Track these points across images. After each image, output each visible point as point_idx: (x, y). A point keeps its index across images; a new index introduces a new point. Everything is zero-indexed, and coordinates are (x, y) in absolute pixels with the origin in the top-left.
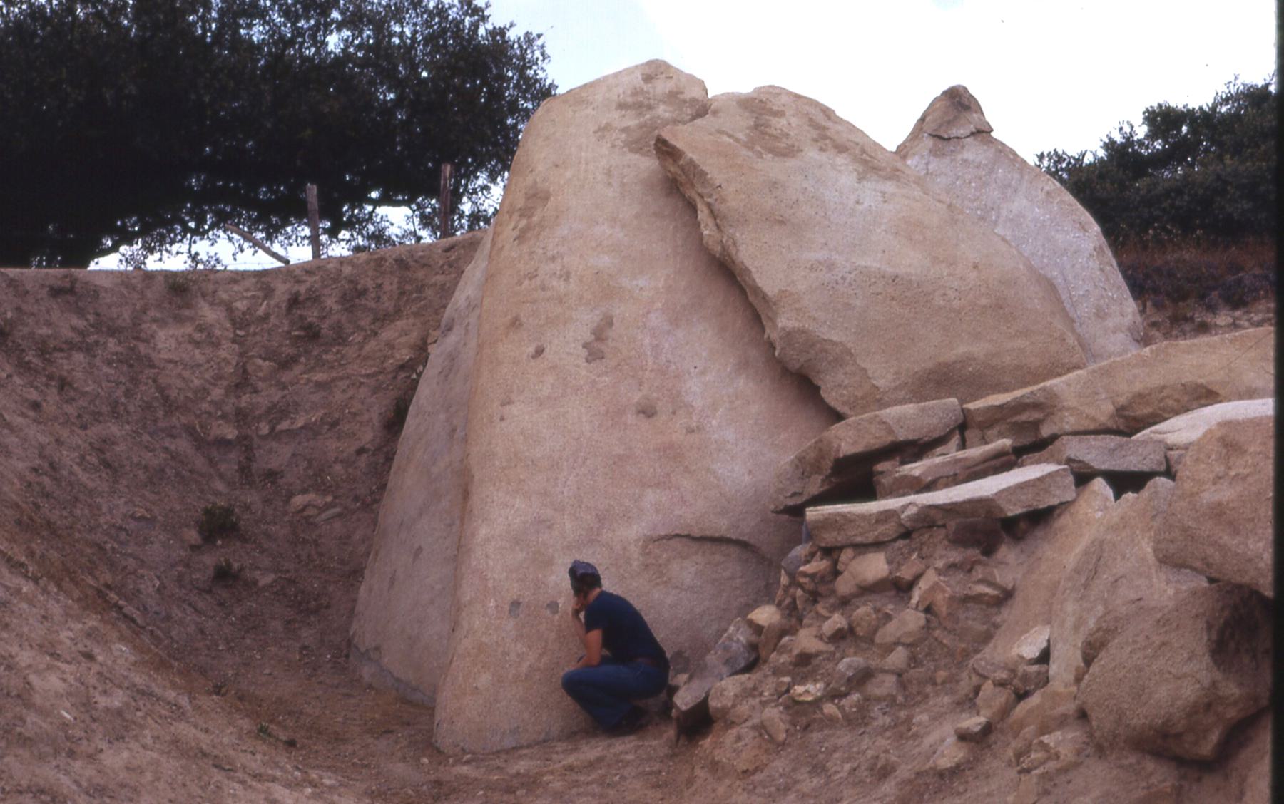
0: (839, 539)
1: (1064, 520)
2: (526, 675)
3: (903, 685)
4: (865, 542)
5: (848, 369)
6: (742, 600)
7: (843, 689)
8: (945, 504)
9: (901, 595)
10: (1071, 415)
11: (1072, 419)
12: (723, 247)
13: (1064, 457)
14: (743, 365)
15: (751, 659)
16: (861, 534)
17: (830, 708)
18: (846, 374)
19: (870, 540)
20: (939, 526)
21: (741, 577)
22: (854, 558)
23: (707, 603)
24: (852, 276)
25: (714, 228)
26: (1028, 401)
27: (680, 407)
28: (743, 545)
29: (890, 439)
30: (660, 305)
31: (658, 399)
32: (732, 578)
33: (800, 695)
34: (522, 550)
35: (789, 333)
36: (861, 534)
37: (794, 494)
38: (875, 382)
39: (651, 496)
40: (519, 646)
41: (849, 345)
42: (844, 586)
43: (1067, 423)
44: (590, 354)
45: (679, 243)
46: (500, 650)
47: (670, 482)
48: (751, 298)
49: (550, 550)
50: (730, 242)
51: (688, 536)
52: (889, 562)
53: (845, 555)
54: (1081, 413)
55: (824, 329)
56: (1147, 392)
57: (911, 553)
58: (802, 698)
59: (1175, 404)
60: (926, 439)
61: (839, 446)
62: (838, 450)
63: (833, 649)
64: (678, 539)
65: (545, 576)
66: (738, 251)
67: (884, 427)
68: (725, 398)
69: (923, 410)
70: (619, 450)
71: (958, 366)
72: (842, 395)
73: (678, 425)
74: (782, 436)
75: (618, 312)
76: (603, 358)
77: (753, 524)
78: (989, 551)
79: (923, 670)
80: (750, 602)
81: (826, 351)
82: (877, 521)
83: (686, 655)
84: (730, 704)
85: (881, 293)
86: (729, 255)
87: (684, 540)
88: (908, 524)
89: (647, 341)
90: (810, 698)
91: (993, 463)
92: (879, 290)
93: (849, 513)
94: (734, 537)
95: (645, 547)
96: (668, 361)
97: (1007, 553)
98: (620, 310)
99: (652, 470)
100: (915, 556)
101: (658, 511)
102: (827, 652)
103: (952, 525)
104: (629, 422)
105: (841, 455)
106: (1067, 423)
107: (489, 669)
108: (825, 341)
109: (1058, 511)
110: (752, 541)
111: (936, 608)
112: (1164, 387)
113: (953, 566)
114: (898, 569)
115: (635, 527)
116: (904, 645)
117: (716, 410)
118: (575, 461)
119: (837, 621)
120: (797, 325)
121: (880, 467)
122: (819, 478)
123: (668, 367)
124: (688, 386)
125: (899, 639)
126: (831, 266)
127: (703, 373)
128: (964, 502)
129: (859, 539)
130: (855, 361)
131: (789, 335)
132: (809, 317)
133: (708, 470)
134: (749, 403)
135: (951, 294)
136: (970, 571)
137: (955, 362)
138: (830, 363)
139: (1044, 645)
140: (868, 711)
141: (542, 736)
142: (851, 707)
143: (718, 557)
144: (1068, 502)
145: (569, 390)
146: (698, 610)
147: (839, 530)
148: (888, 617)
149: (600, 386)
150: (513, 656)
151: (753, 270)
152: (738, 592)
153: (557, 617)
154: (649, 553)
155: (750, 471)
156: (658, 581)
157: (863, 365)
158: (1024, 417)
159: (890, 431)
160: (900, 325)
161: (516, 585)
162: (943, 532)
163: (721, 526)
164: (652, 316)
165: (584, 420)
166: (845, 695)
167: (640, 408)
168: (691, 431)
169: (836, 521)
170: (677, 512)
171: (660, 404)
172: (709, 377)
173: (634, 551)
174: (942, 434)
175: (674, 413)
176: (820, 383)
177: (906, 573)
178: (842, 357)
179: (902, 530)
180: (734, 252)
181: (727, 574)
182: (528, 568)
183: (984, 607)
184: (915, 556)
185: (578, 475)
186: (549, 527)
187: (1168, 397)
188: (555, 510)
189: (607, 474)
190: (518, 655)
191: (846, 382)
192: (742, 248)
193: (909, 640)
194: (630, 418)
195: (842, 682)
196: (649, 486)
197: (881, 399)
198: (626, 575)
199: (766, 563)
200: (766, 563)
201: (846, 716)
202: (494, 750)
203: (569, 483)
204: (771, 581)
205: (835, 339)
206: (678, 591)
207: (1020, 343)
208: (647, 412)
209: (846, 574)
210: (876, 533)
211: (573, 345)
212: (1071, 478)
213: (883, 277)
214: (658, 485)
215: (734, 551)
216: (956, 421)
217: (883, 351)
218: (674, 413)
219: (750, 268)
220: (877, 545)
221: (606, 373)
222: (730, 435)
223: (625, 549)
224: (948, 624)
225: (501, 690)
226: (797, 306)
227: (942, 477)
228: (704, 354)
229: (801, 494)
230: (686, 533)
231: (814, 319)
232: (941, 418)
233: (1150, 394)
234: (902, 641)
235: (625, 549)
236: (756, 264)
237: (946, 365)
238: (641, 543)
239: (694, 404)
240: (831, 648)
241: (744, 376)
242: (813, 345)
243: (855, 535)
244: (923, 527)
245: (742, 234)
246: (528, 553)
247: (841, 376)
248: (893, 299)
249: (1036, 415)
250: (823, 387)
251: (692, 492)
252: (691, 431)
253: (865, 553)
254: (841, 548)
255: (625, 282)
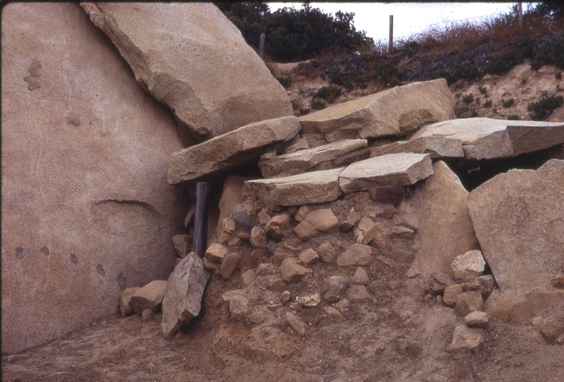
0: (300, 200)
1: (433, 186)
2: (35, 297)
3: (371, 291)
4: (319, 202)
5: (191, 99)
6: (148, 239)
7: (338, 297)
8: (371, 178)
9: (343, 234)
10: (381, 125)
11: (381, 128)
12: (105, 22)
13: (424, 149)
14: (123, 95)
15: (208, 278)
16: (316, 197)
17: (330, 310)
18: (189, 102)
19: (323, 201)
20: (363, 191)
21: (146, 225)
22: (308, 212)
23: (131, 243)
24: (184, 44)
25: (98, 10)
26: (354, 117)
27: (94, 121)
28: (144, 205)
29: (272, 139)
30: (68, 56)
31: (79, 115)
32: (141, 226)
33: (308, 302)
34: (16, 213)
35: (159, 76)
36: (316, 197)
37: (189, 173)
38: (205, 107)
39: (90, 176)
40: (27, 278)
41: (191, 85)
42: (303, 229)
43: (379, 130)
44: (30, 85)
45: (68, 19)
46: (14, 281)
47: (98, 167)
48: (123, 55)
49: (36, 213)
50: (111, 19)
51: (115, 201)
52: (336, 214)
53: (302, 211)
54: (386, 124)
55: (177, 74)
56: (406, 114)
57: (350, 207)
58: (310, 305)
59: (418, 120)
60: (288, 139)
61: (243, 143)
62: (242, 146)
63: (311, 271)
64: (109, 203)
65: (36, 230)
66: (117, 25)
67: (268, 131)
68: (118, 115)
69: (283, 122)
70: (63, 147)
71: (239, 99)
72: (188, 115)
73: (195, 125)
74: (153, 139)
75: (43, 59)
76: (39, 88)
77: (148, 192)
78: (397, 205)
79: (380, 281)
80: (153, 240)
81: (179, 88)
82: (328, 189)
83: (124, 275)
84: (246, 311)
85: (200, 55)
86: (110, 27)
87: (113, 203)
88: (345, 190)
89: (65, 78)
90: (315, 304)
91: (359, 153)
92: (198, 53)
93: (309, 184)
94: (140, 201)
95: (92, 209)
96: (80, 91)
97: (405, 206)
98: (43, 58)
99: (86, 159)
100: (352, 210)
101: (96, 186)
102: (309, 273)
103: (374, 190)
104: (65, 128)
105: (244, 149)
106: (379, 130)
107: (8, 295)
108: (178, 81)
109: (428, 181)
110: (150, 203)
111: (377, 242)
112: (412, 111)
113: (379, 216)
114: (345, 216)
115: (84, 196)
116: (361, 266)
117: (115, 122)
118: (38, 154)
119: (309, 254)
120: (162, 71)
121: (268, 155)
122: (211, 164)
123: (81, 95)
124: (95, 107)
125: (357, 262)
126: (171, 38)
127: (102, 99)
128: (386, 176)
129: (314, 200)
130: (194, 94)
131: (159, 78)
132: (168, 67)
133: (119, 159)
134: (132, 119)
135: (230, 59)
136: (391, 218)
137: (238, 97)
138: (180, 95)
139: (484, 263)
140: (357, 310)
141: (51, 338)
142: (344, 308)
143: (132, 213)
144: (432, 175)
145: (22, 108)
146: (127, 247)
147: (300, 195)
148: (342, 249)
149: (42, 106)
150: (24, 285)
151: (130, 37)
152: (145, 235)
153: (49, 257)
154: (95, 213)
155: (141, 160)
156: (104, 230)
157: (198, 97)
158: (351, 126)
159: (273, 134)
160: (212, 75)
161: (17, 237)
162: (367, 194)
163: (132, 194)
164: (65, 63)
165: (37, 127)
166: (338, 300)
167: (70, 121)
168: (103, 135)
169: (299, 189)
170: (106, 186)
171: (81, 118)
172: (106, 102)
173: (87, 211)
174: (294, 136)
175: (91, 123)
176: (175, 107)
177: (350, 221)
178: (187, 92)
179: (340, 194)
180: (114, 25)
181: (139, 224)
182: (23, 225)
183: (405, 240)
184: (352, 210)
185: (42, 163)
186: (31, 197)
187: (415, 116)
188: (33, 186)
189: (59, 162)
190: (27, 284)
191: (190, 107)
192: (119, 23)
193: (365, 263)
194: (66, 127)
195: (337, 292)
196: (87, 169)
197: (209, 117)
198: (85, 227)
199: (157, 216)
200: (157, 216)
201: (343, 314)
202: (21, 349)
203: (37, 168)
204: (161, 227)
205: (183, 80)
206: (115, 236)
207: (262, 88)
208: (75, 123)
209: (304, 223)
210: (327, 196)
211: (17, 79)
212: (430, 161)
213: (199, 46)
214: (92, 169)
215: (140, 209)
216: (298, 129)
217: (206, 90)
218: (91, 123)
219: (128, 35)
220: (326, 204)
221: (43, 98)
222: (125, 137)
223: (81, 210)
224: (386, 252)
225: (19, 309)
226: (160, 60)
227: (323, 161)
228: (100, 87)
229: (193, 173)
230: (114, 199)
231: (171, 68)
232: (292, 127)
233: (407, 115)
234: (360, 263)
235: (81, 210)
236: (130, 33)
237: (234, 99)
238: (90, 206)
239: (101, 118)
240: (309, 270)
241: (125, 102)
242: (172, 84)
243: (313, 198)
244: (353, 192)
245: (118, 15)
246: (21, 215)
247: (187, 103)
248: (206, 59)
249: (357, 126)
250: (177, 110)
251: (113, 173)
252: (103, 135)
253: (316, 209)
254: (298, 207)
255: (43, 40)
